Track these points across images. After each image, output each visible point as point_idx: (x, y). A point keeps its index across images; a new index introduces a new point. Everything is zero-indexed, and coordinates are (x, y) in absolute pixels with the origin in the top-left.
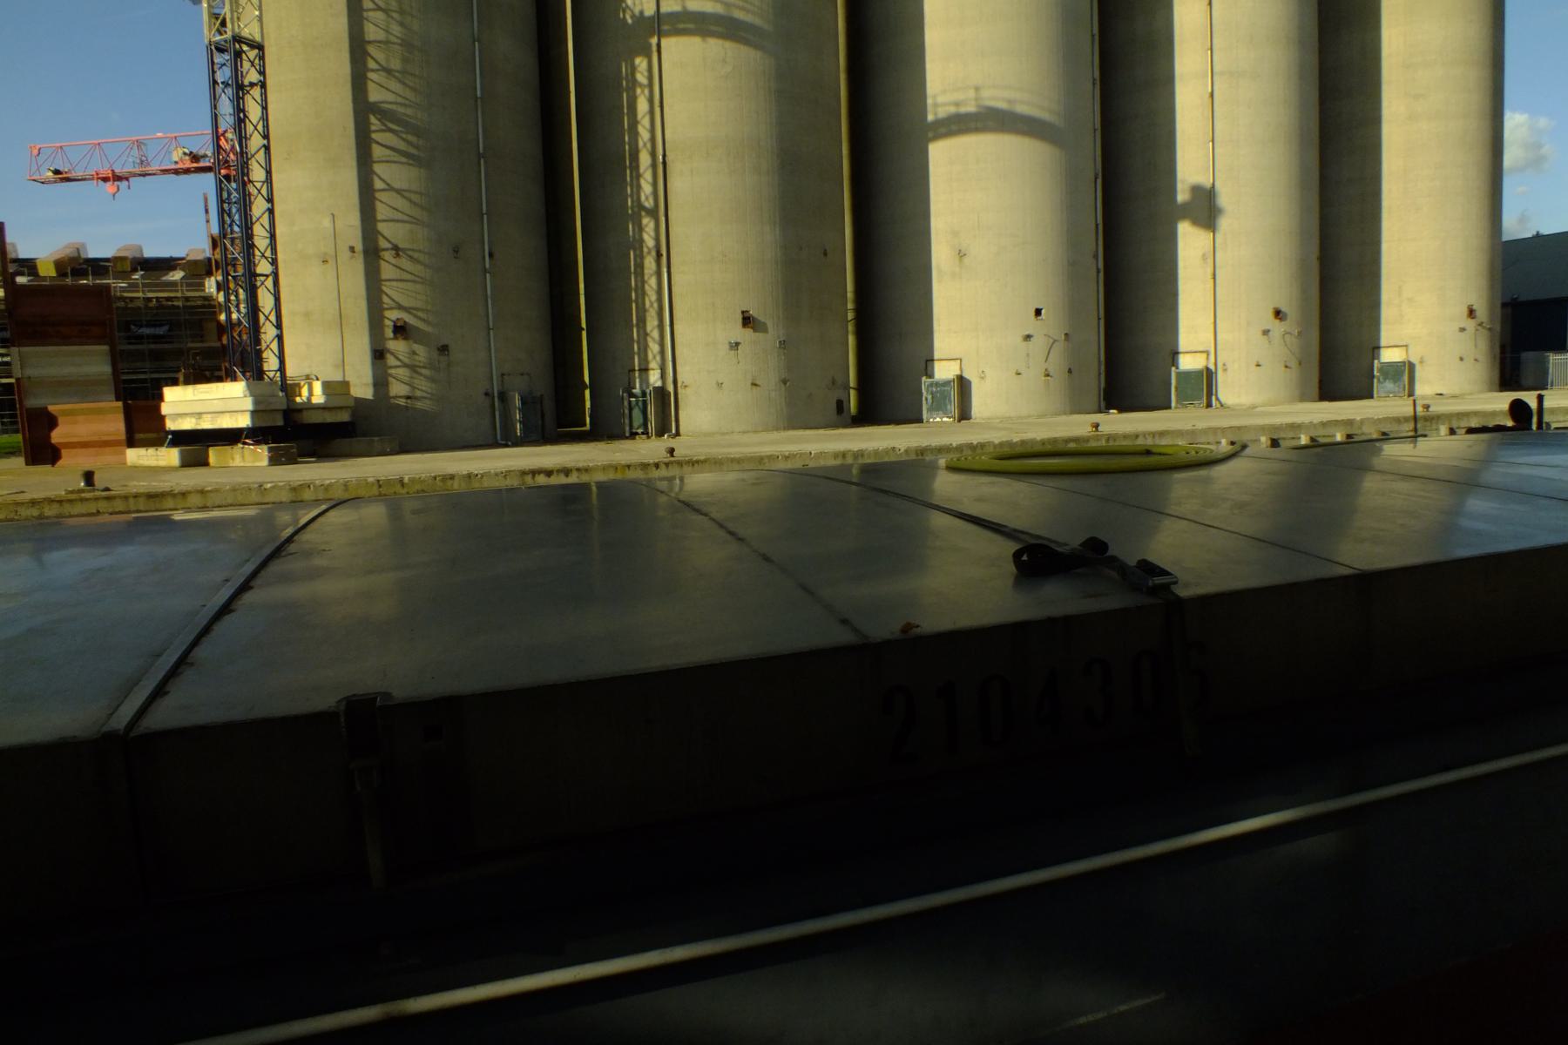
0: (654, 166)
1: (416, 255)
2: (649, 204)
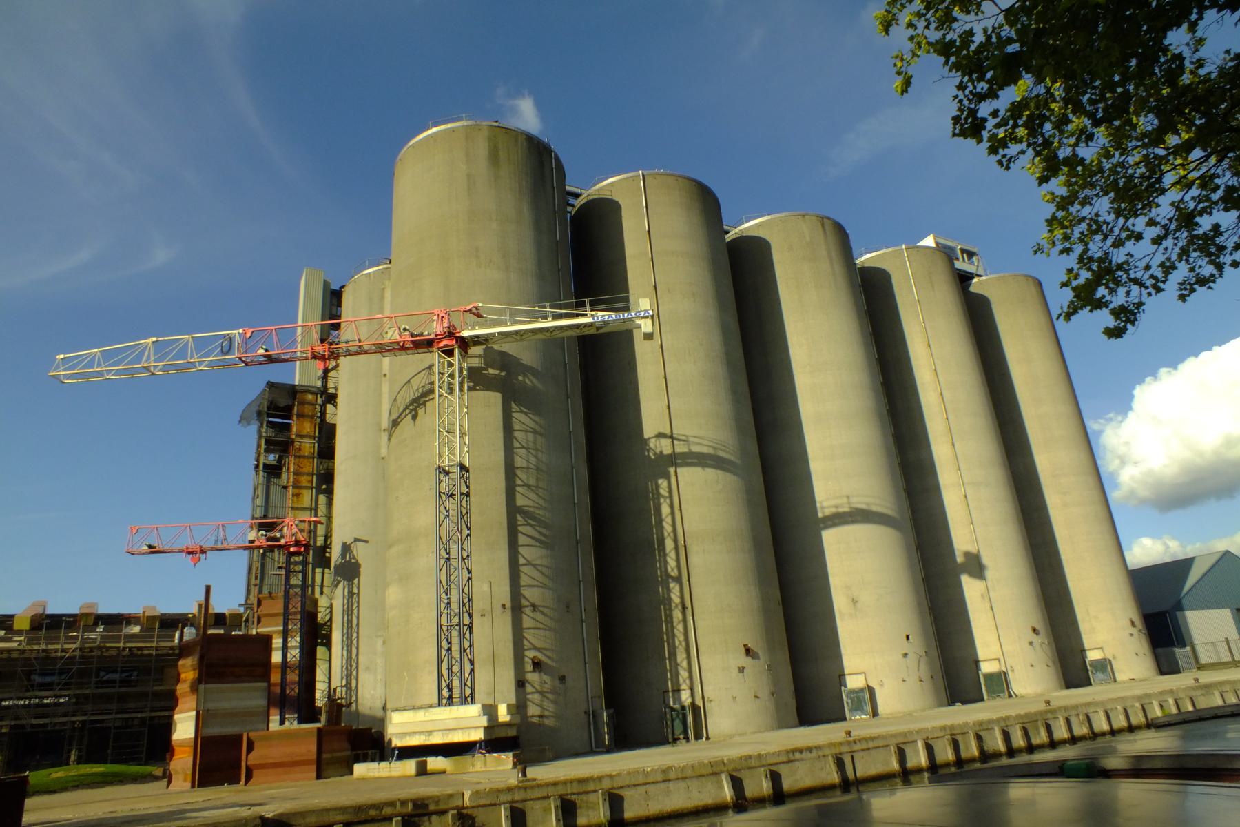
0: (676, 548)
1: (545, 610)
2: (674, 573)
